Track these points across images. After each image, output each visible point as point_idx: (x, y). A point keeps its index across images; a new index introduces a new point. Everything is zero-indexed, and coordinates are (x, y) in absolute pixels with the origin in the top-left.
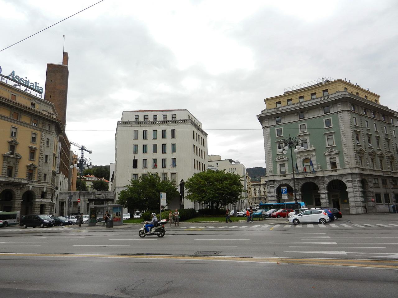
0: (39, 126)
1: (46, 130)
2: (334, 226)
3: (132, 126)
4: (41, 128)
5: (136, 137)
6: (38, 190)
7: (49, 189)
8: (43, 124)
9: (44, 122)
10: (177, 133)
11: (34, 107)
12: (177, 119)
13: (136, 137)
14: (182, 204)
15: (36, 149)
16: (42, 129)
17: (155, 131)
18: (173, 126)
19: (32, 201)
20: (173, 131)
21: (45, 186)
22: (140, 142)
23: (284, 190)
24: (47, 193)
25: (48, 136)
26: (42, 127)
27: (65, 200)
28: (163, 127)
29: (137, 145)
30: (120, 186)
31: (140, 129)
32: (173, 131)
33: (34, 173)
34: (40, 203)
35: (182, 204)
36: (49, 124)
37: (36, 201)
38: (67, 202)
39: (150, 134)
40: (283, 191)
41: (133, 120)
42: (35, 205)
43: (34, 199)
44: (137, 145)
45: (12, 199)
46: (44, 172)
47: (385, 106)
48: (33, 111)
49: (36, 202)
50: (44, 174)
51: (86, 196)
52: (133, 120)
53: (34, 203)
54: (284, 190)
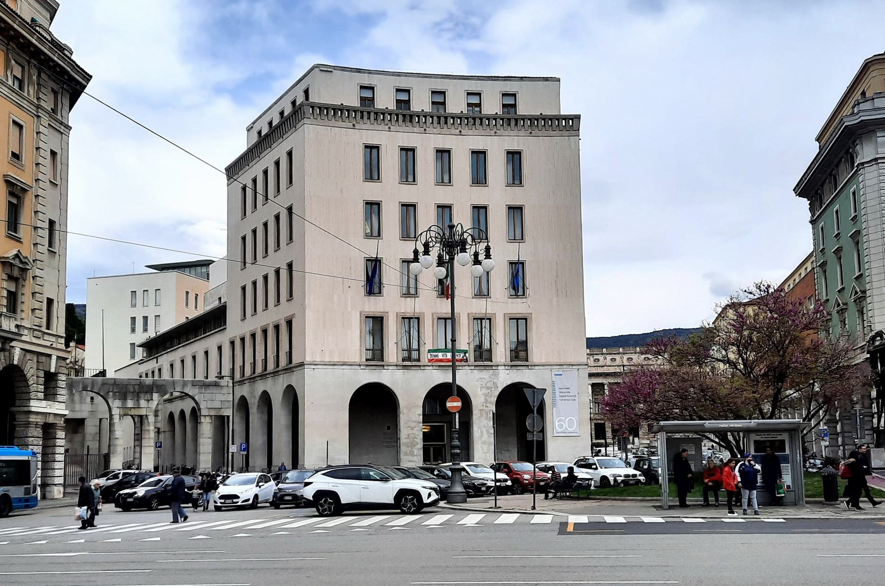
2: (648, 487)
3: (357, 126)
5: (372, 172)
12: (522, 110)
13: (372, 172)
17: (408, 152)
18: (514, 140)
22: (391, 192)
28: (477, 140)
29: (414, 206)
30: (318, 359)
31: (391, 140)
32: (514, 157)
33: (23, 294)
34: (40, 420)
36: (56, 87)
37: (33, 409)
39: (426, 164)
41: (355, 103)
42: (28, 424)
43: (18, 403)
44: (414, 206)
47: (812, 150)
51: (129, 396)
52: (355, 103)
53: (21, 418)
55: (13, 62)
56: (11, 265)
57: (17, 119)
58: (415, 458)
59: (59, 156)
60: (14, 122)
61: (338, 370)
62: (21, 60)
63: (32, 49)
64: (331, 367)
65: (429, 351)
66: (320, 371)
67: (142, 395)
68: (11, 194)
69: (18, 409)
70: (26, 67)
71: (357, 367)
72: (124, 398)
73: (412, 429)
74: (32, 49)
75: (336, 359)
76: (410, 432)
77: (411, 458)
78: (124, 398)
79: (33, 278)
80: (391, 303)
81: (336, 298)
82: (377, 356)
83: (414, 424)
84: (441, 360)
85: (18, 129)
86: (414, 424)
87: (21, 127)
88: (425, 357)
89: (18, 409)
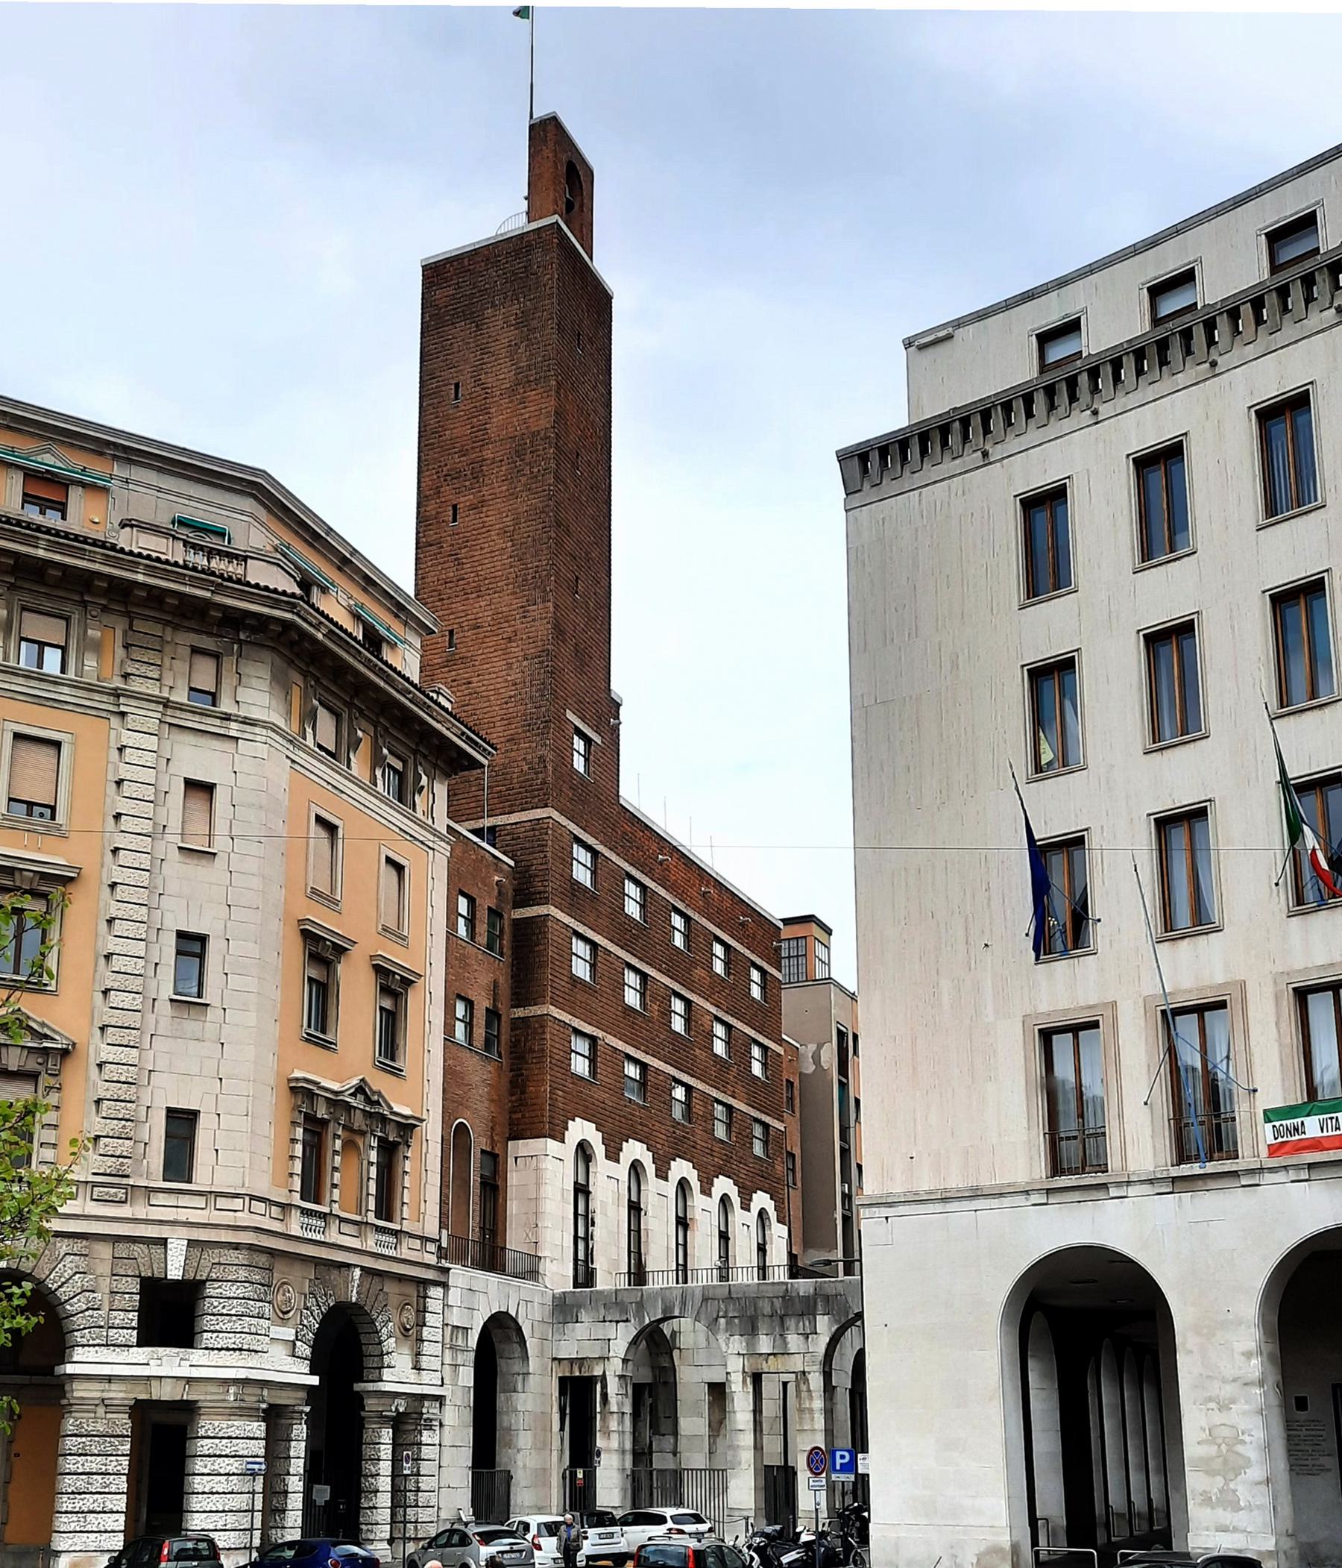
0: (79, 672)
1: (166, 704)
4: (118, 683)
6: (104, 1268)
7: (233, 1256)
8: (127, 647)
9: (138, 625)
10: (1332, 431)
11: (64, 518)
14: (609, 1563)
15: (67, 881)
16: (116, 694)
19: (359, 1387)
20: (1285, 419)
21: (173, 1223)
23: (843, 1457)
24: (210, 1291)
25: (198, 758)
26: (126, 676)
27: (598, 1371)
30: (898, 1187)
35: (609, 1563)
37: (70, 1369)
38: (613, 1386)
40: (839, 1461)
45: (64, 1397)
46: (170, 1092)
48: (53, 547)
49: (73, 1377)
50: (172, 1114)
51: (763, 1327)
54: (843, 1457)
55: (385, 751)
56: (349, 1107)
57: (391, 855)
58: (1241, 1519)
59: (407, 870)
60: (319, 820)
61: (961, 1215)
62: (400, 749)
63: (350, 678)
64: (938, 1207)
65: (1269, 1115)
66: (908, 1222)
67: (791, 1323)
68: (385, 990)
69: (371, 1387)
70: (345, 716)
71: (1020, 1200)
72: (751, 1331)
73: (1224, 1407)
74: (350, 678)
75: (955, 1182)
76: (1218, 1418)
77: (1225, 1517)
78: (751, 1331)
79: (100, 1066)
80: (1126, 968)
81: (946, 985)
82: (1073, 1148)
83: (1228, 1391)
84: (1316, 1145)
85: (393, 873)
86: (1228, 1391)
87: (399, 869)
88: (1255, 1136)
89: (371, 1387)
